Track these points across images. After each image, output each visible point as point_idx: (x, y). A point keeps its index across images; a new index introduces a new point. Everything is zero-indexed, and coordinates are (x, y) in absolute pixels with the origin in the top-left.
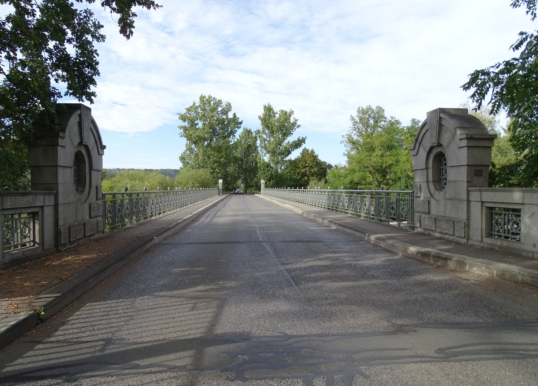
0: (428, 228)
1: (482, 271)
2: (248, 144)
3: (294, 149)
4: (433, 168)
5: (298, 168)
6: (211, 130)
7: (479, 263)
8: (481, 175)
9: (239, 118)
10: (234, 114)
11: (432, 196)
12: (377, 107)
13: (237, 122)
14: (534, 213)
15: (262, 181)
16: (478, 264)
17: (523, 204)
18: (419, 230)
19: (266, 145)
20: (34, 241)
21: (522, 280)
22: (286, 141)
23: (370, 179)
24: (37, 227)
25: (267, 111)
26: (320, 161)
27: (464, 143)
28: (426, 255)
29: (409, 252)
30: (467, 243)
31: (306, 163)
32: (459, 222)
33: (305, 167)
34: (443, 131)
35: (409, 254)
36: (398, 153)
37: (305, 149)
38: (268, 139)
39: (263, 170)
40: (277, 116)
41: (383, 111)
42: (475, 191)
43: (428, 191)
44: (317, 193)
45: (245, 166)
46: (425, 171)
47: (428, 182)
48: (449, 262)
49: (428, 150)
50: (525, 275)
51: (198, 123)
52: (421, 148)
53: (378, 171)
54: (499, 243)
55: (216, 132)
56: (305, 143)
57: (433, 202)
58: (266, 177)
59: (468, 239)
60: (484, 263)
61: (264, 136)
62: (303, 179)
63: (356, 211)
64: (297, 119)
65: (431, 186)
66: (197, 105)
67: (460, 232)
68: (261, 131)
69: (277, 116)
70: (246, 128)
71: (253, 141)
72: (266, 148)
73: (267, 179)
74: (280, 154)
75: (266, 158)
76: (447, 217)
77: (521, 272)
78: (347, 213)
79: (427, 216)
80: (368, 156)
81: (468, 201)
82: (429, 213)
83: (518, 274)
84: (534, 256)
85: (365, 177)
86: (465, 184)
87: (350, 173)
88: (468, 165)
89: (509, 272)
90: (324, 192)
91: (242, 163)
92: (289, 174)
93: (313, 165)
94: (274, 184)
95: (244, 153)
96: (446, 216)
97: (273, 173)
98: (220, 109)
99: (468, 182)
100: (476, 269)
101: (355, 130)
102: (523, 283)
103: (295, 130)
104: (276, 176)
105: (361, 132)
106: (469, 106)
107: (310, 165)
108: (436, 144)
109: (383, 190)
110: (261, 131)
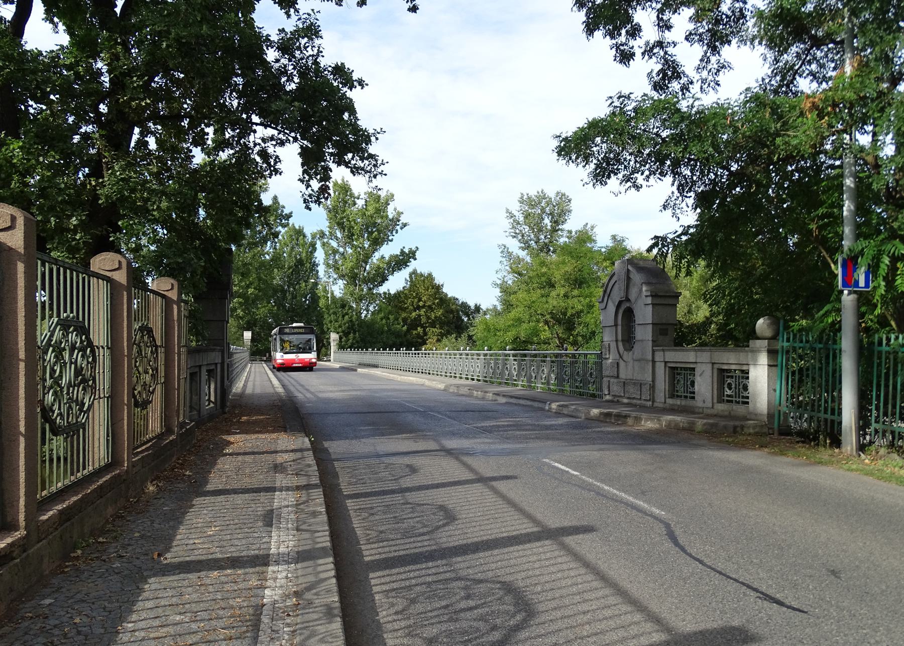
0: (617, 394)
1: (655, 424)
2: (296, 257)
3: (393, 271)
4: (622, 325)
5: (404, 309)
8: (667, 334)
9: (284, 207)
10: (275, 198)
11: (621, 357)
12: (558, 193)
13: (281, 215)
15: (334, 337)
17: (696, 363)
18: (608, 397)
19: (336, 262)
22: (377, 255)
23: (546, 334)
24: (212, 386)
25: (339, 194)
26: (446, 295)
27: (649, 300)
28: (608, 415)
31: (420, 300)
32: (646, 384)
33: (419, 308)
34: (631, 284)
36: (591, 293)
37: (414, 272)
38: (341, 250)
40: (360, 203)
41: (570, 201)
44: (443, 356)
45: (291, 304)
46: (614, 328)
47: (617, 341)
52: (610, 301)
53: (559, 321)
56: (415, 259)
57: (622, 364)
58: (340, 326)
59: (653, 402)
61: (334, 244)
62: (414, 332)
63: (529, 381)
64: (401, 211)
65: (620, 344)
67: (646, 395)
68: (327, 233)
69: (360, 203)
70: (293, 224)
71: (307, 252)
72: (338, 269)
73: (343, 332)
74: (366, 281)
75: (338, 289)
78: (517, 385)
79: (616, 380)
80: (542, 296)
81: (654, 362)
82: (618, 377)
85: (537, 331)
86: (650, 343)
87: (513, 325)
88: (652, 324)
90: (478, 355)
91: (284, 297)
92: (384, 321)
93: (434, 303)
94: (357, 342)
95: (288, 277)
97: (354, 320)
101: (515, 237)
103: (397, 233)
104: (360, 325)
105: (527, 242)
107: (429, 303)
110: (327, 233)
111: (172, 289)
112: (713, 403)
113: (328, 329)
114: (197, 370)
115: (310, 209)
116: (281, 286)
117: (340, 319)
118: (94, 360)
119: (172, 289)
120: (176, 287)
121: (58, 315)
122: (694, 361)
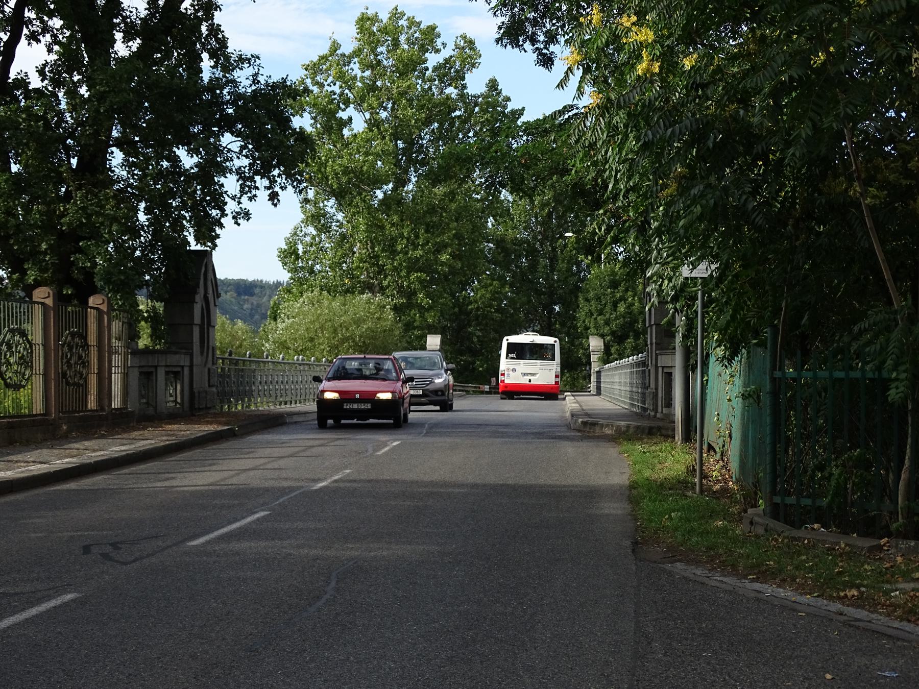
6: (400, 144)
10: (493, 85)
15: (595, 343)
20: (175, 401)
24: (179, 387)
39: (598, 299)
51: (350, 119)
55: (419, 152)
66: (348, 47)
73: (613, 333)
91: (533, 266)
98: (433, 60)
111: (103, 303)
113: (587, 328)
114: (153, 369)
115: (239, 225)
116: (528, 242)
117: (608, 308)
118: (32, 351)
119: (103, 303)
120: (106, 302)
121: (9, 326)
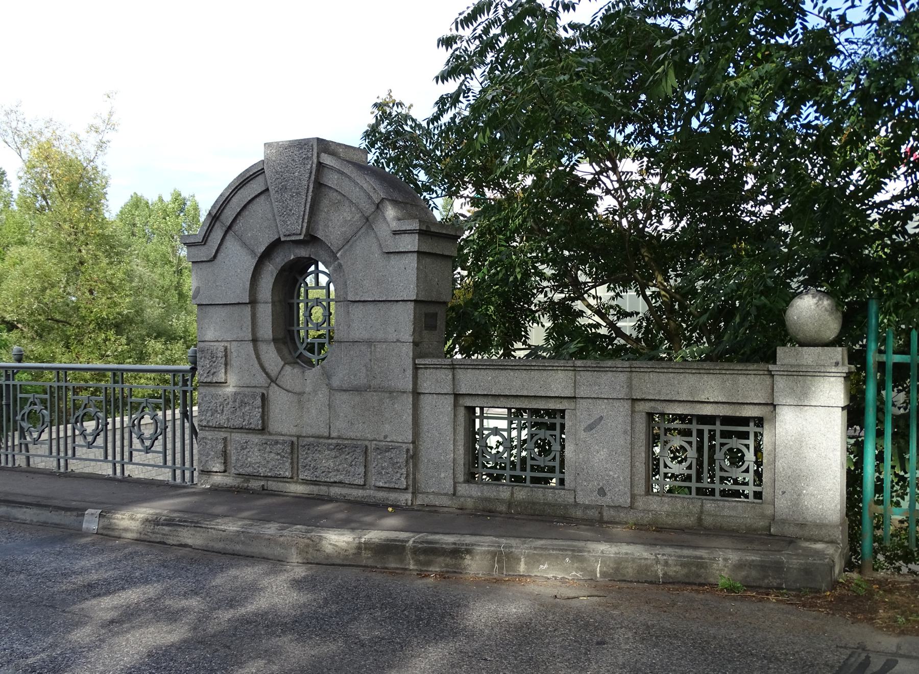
1: (565, 570)
7: (553, 549)
14: (601, 418)
16: (550, 555)
17: (575, 398)
21: (665, 574)
27: (411, 243)
29: (329, 549)
30: (412, 504)
34: (325, 203)
35: (328, 556)
42: (436, 367)
43: (257, 366)
48: (468, 561)
49: (262, 249)
50: (670, 562)
52: (232, 245)
54: (504, 493)
60: (566, 550)
76: (339, 438)
77: (659, 556)
81: (416, 394)
82: (263, 430)
83: (654, 562)
84: (602, 516)
86: (407, 350)
89: (633, 560)
96: (334, 434)
99: (416, 344)
100: (546, 566)
102: (669, 581)
106: (22, 117)
108: (302, 237)
109: (19, 361)
112: (633, 497)
122: (568, 393)
